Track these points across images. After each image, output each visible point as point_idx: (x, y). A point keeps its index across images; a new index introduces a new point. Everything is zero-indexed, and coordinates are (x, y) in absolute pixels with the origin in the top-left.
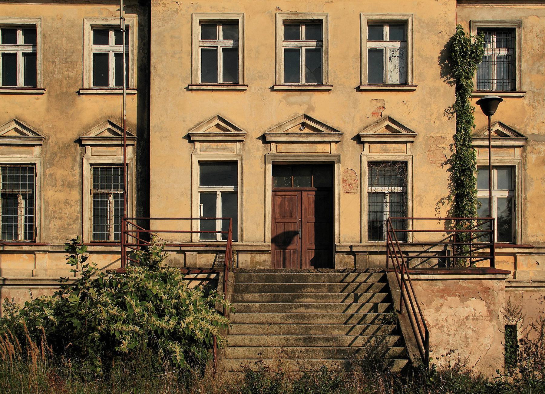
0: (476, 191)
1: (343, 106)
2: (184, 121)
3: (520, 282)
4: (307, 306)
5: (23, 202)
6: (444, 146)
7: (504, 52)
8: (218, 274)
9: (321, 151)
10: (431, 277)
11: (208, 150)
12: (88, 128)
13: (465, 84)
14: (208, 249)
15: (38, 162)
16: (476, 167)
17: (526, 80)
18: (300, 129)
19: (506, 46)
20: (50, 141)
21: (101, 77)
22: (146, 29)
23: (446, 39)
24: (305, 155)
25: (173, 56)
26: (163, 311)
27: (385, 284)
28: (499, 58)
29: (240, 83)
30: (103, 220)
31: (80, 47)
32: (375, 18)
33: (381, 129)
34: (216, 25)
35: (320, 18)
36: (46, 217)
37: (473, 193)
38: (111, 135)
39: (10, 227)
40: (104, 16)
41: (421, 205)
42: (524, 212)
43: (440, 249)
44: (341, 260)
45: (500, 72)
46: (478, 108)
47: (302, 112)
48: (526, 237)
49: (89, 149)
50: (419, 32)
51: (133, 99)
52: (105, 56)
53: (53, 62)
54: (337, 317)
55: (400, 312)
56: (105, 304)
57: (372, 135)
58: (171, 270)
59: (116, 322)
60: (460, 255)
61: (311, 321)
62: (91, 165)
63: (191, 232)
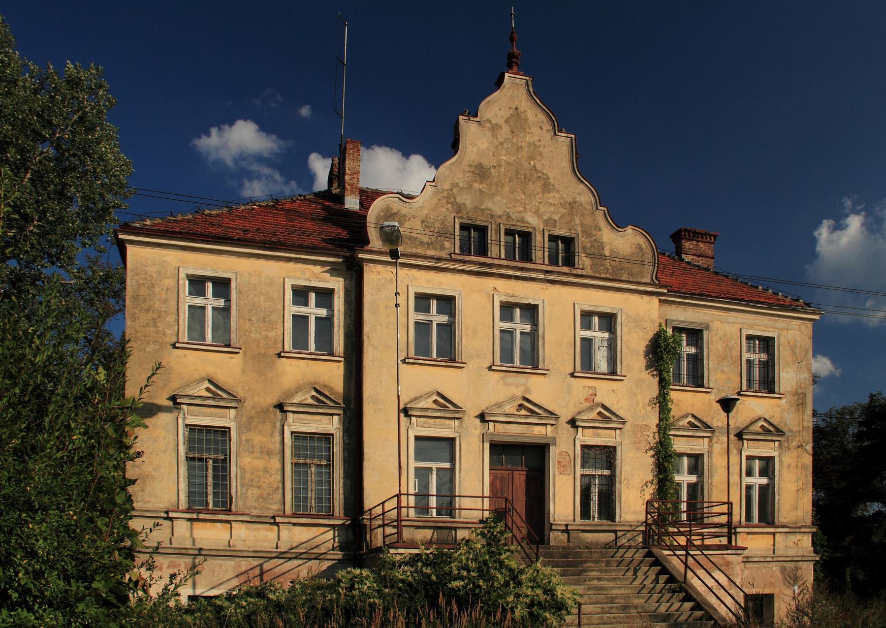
1: (556, 389)
9: (538, 433)
12: (291, 394)
15: (232, 425)
17: (713, 378)
18: (517, 410)
20: (246, 404)
21: (300, 341)
23: (650, 335)
24: (522, 435)
25: (387, 327)
29: (458, 360)
31: (281, 307)
33: (593, 415)
35: (536, 303)
36: (242, 485)
40: (307, 277)
44: (556, 538)
49: (290, 415)
51: (339, 367)
52: (305, 318)
53: (250, 320)
61: (609, 592)
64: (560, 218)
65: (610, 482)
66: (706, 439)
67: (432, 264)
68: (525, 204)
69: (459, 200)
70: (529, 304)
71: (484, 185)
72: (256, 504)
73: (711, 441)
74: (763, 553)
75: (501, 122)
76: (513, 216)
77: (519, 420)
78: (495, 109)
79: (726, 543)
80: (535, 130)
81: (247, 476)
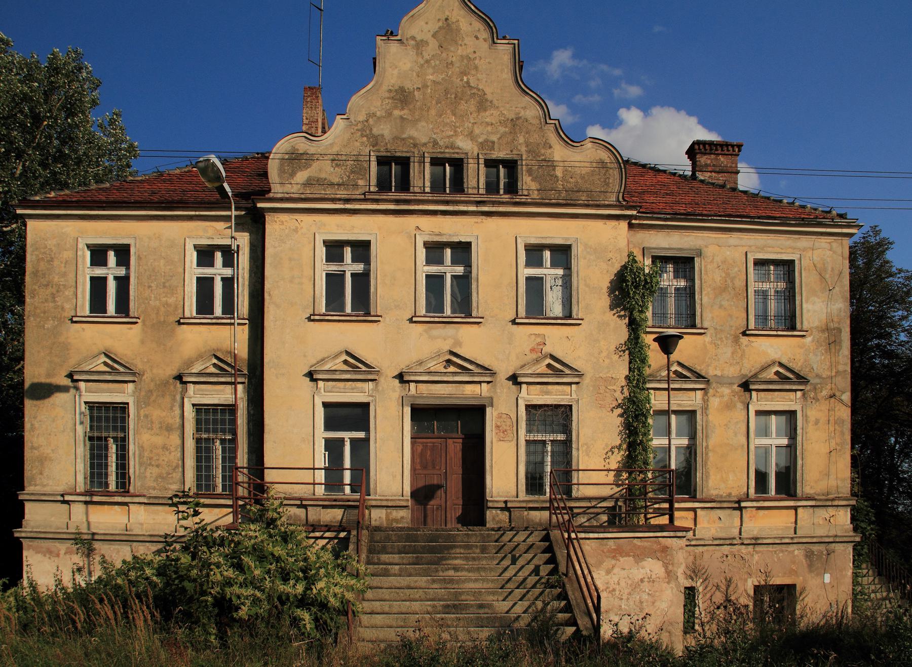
0: (651, 440)
1: (495, 339)
2: (305, 356)
3: (700, 539)
4: (456, 569)
5: (114, 447)
6: (614, 387)
7: (682, 283)
8: (349, 532)
9: (470, 393)
10: (601, 535)
11: (334, 390)
12: (190, 363)
13: (638, 319)
14: (334, 503)
16: (651, 412)
17: (708, 315)
18: (445, 367)
19: (685, 277)
20: (144, 377)
21: (205, 304)
22: (259, 250)
23: (617, 267)
25: (291, 282)
26: (288, 574)
27: (547, 544)
28: (677, 289)
29: (372, 313)
30: (209, 468)
31: (181, 270)
32: (533, 241)
33: (542, 368)
34: (343, 247)
36: (141, 464)
37: (648, 441)
38: (218, 372)
39: (100, 475)
40: (209, 235)
41: (588, 455)
42: (706, 463)
43: (610, 504)
45: (677, 307)
46: (655, 346)
47: (447, 348)
48: (708, 490)
49: (191, 387)
50: (585, 258)
51: (243, 330)
52: (211, 280)
53: (150, 287)
54: (492, 581)
55: (566, 575)
56: (218, 565)
57: (531, 375)
58: (292, 528)
59: (232, 585)
60: (634, 510)
62: (194, 405)
63: (314, 484)
64: (499, 139)
65: (565, 449)
66: (698, 392)
67: (342, 206)
68: (456, 127)
69: (375, 131)
70: (460, 243)
71: (406, 111)
72: (155, 484)
73: (706, 394)
74: (780, 533)
75: (428, 37)
76: (441, 143)
77: (445, 379)
78: (421, 23)
79: (667, 522)
80: (469, 41)
81: (146, 454)
